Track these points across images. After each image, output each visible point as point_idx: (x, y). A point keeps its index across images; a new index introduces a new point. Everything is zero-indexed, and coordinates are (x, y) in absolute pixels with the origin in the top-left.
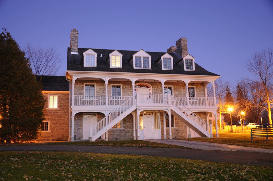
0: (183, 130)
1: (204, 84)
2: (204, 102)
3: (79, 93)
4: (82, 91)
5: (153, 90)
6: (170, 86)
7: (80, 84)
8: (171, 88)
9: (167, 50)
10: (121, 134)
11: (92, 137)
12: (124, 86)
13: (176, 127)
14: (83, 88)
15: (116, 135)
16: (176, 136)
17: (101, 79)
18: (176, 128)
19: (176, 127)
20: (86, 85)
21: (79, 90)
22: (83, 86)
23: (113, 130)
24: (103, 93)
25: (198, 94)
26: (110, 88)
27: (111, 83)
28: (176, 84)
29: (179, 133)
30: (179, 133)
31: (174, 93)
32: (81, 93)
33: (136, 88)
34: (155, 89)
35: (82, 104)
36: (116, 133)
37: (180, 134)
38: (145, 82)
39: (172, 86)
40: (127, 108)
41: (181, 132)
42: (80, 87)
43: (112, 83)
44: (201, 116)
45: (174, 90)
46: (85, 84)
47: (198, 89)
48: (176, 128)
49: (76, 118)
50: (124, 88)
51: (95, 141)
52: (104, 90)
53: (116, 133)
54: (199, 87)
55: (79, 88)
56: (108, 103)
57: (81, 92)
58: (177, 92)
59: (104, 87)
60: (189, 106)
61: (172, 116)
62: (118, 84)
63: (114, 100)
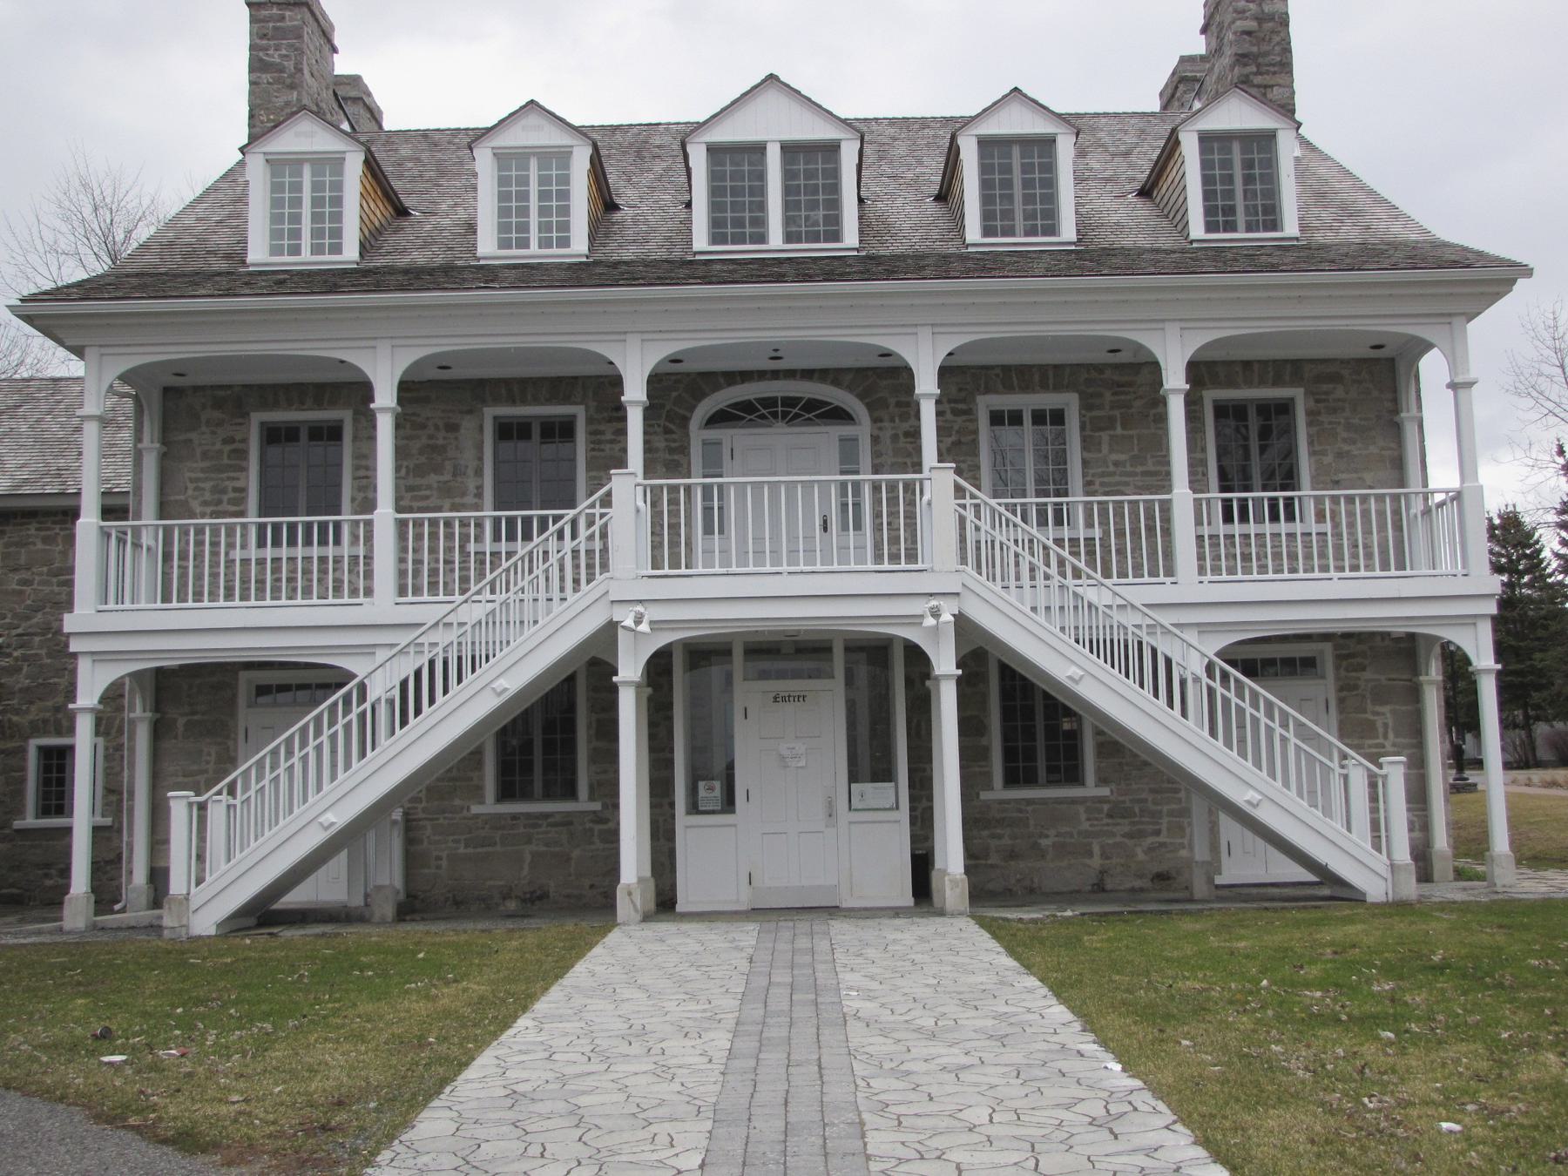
0: (1171, 813)
1: (1391, 362)
2: (1367, 532)
3: (205, 503)
4: (230, 484)
5: (875, 440)
6: (1047, 400)
7: (220, 424)
8: (1058, 417)
9: (1184, 60)
10: (576, 853)
11: (187, 897)
12: (610, 420)
13: (1102, 781)
14: (242, 454)
15: (528, 858)
16: (1103, 872)
17: (887, 354)
18: (1105, 791)
19: (592, 798)
20: (997, 418)
21: (203, 470)
22: (245, 440)
23: (500, 816)
24: (418, 488)
25: (1328, 459)
26: (480, 447)
27: (484, 402)
28: (1108, 374)
29: (1130, 835)
30: (1130, 835)
31: (1085, 463)
32: (225, 498)
33: (713, 434)
34: (895, 438)
35: (1385, 566)
36: (533, 847)
37: (1151, 849)
38: (808, 374)
39: (1070, 402)
40: (522, 622)
41: (1158, 833)
42: (218, 446)
43: (497, 401)
44: (1367, 675)
45: (1084, 440)
46: (490, 412)
47: (1334, 411)
48: (1105, 791)
49: (181, 721)
50: (609, 436)
51: (212, 931)
52: (423, 459)
53: (533, 847)
54: (1340, 392)
55: (205, 456)
56: (402, 574)
57: (223, 491)
58: (1115, 457)
59: (424, 440)
60: (1188, 583)
61: (969, 684)
62: (549, 401)
63: (1237, 528)
